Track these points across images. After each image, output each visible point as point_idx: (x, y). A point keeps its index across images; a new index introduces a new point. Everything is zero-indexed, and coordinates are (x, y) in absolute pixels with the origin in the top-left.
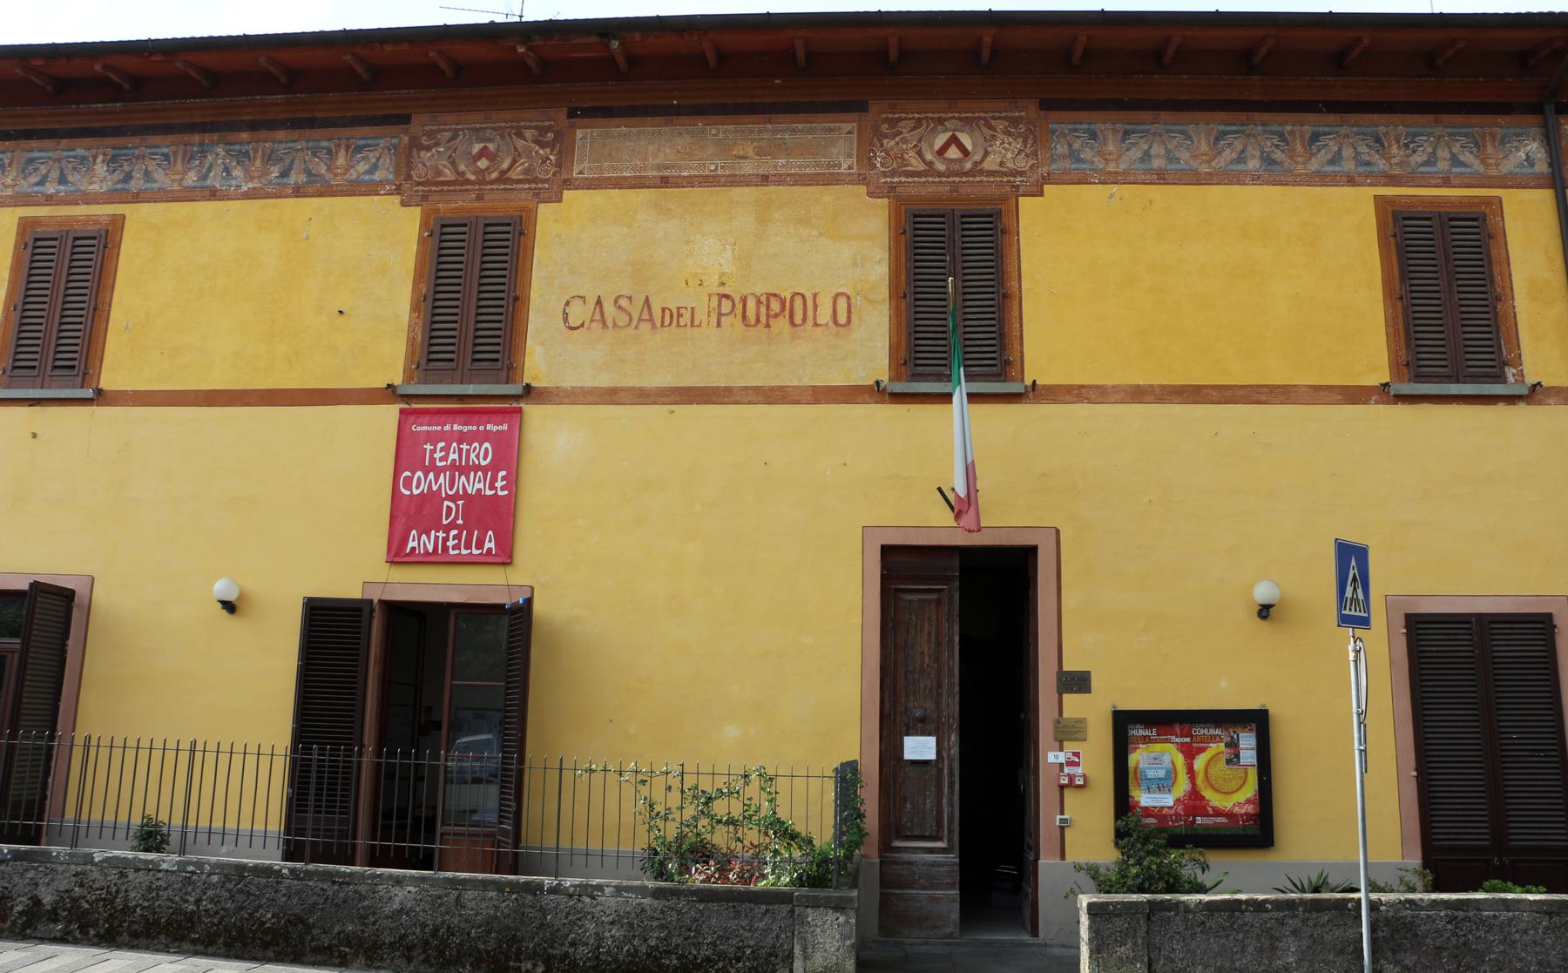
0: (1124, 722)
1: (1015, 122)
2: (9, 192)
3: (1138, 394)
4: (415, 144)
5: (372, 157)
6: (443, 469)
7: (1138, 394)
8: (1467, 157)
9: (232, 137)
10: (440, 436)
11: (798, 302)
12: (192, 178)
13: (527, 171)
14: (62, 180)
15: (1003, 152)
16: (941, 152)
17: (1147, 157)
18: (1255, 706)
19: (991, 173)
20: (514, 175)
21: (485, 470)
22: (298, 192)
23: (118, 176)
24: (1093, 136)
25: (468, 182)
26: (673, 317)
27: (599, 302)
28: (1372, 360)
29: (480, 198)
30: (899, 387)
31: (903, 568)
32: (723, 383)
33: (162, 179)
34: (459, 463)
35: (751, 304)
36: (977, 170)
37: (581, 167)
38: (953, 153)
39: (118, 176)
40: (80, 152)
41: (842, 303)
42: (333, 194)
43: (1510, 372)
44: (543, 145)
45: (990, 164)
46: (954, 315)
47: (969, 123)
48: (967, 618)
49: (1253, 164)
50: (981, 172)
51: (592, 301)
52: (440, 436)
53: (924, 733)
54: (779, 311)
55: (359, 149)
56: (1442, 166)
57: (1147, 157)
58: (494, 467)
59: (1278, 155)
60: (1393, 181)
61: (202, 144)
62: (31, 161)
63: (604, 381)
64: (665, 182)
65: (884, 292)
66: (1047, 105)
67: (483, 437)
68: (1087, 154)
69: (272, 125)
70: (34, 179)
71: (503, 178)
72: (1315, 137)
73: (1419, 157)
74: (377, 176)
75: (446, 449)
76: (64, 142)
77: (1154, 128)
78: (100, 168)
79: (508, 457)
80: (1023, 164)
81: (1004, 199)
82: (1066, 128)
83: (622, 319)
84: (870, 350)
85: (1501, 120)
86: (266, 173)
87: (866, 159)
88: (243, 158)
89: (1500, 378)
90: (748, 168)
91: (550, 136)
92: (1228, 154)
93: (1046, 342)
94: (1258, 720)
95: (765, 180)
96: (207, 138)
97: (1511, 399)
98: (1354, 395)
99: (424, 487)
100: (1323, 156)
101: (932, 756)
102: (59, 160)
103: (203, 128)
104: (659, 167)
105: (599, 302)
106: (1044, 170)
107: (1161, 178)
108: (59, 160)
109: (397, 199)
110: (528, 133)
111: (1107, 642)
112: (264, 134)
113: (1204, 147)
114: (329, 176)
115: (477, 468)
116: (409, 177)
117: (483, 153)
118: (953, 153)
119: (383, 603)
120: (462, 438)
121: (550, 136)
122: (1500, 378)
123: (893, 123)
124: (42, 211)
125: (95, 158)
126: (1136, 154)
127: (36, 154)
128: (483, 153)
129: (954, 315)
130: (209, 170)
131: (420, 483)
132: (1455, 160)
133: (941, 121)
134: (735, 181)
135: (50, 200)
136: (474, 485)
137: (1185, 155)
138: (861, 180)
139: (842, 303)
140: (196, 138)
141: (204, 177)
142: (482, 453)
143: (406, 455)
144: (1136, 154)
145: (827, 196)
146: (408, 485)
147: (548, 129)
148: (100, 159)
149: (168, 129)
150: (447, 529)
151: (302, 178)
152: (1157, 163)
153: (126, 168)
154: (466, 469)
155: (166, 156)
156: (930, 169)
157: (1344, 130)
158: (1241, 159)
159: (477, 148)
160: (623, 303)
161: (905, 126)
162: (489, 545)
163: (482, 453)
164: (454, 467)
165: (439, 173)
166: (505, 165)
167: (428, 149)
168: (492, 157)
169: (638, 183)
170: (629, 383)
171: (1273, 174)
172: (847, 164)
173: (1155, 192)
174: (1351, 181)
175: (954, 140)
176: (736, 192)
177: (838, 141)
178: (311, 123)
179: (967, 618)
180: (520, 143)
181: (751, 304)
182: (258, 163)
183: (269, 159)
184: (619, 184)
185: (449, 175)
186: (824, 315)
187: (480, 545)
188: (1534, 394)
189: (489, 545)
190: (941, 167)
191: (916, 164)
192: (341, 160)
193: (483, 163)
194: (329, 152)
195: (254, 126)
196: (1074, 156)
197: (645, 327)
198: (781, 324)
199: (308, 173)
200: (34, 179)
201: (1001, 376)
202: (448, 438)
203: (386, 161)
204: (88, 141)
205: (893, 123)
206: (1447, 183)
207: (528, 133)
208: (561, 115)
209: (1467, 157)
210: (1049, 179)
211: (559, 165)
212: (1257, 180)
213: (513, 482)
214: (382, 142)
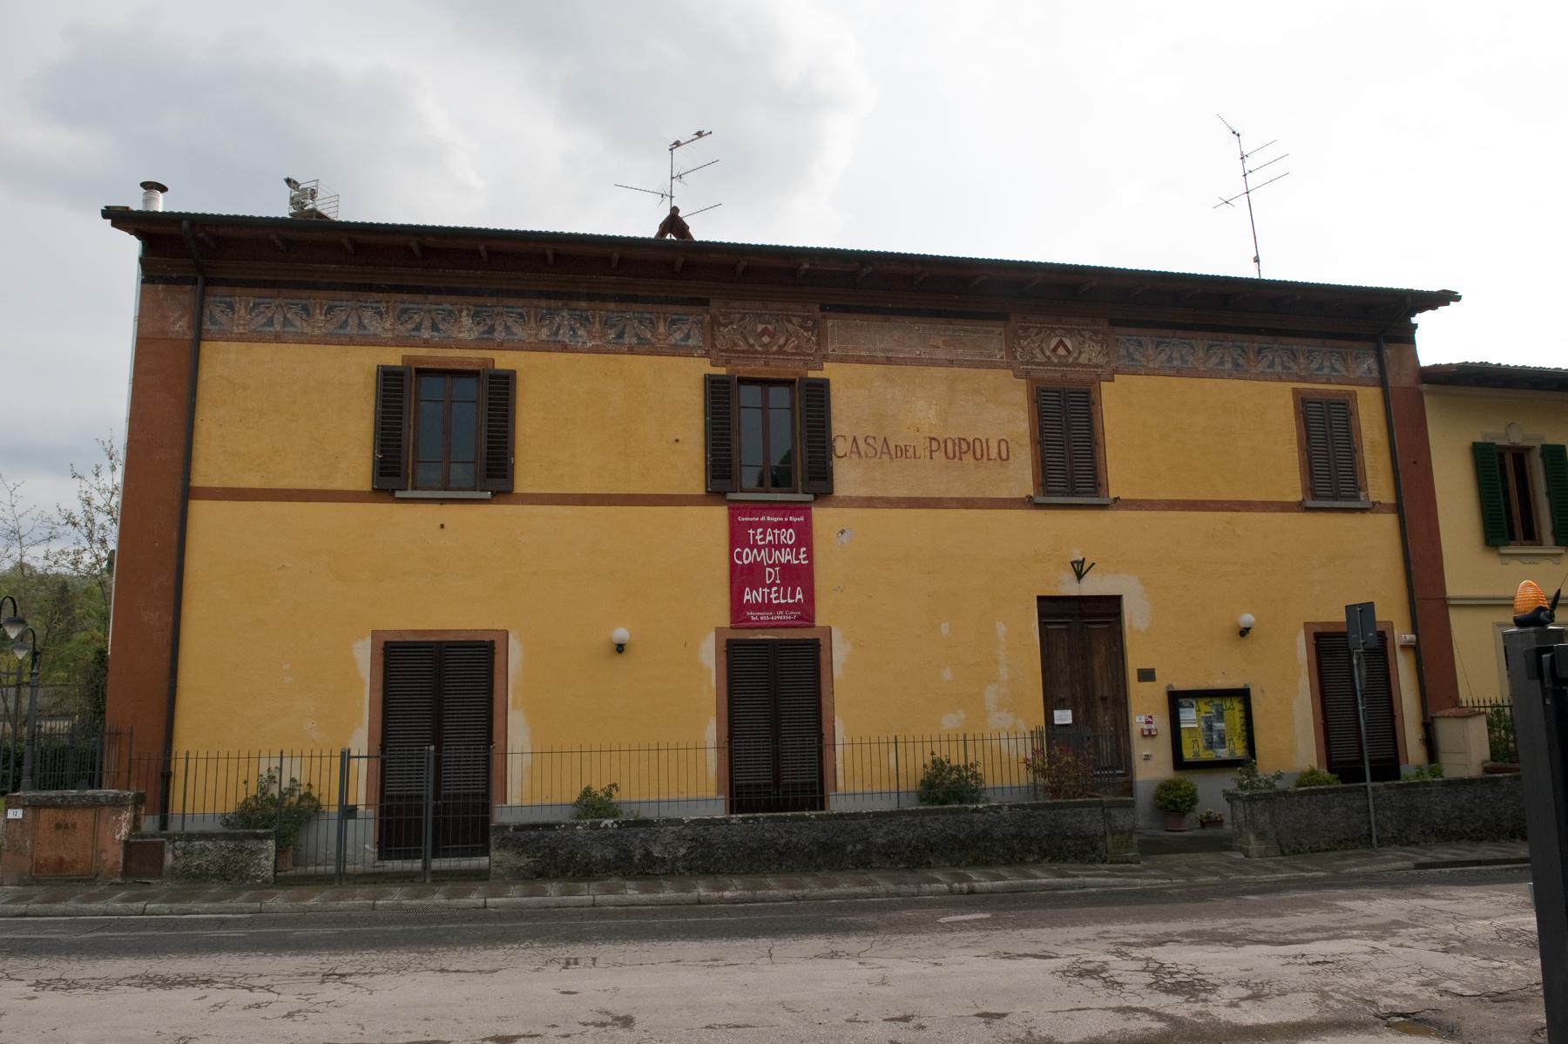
0: (1176, 699)
1: (1096, 332)
2: (390, 335)
3: (1172, 505)
4: (715, 322)
5: (685, 328)
6: (764, 546)
7: (1172, 505)
8: (1338, 366)
9: (574, 304)
10: (759, 524)
11: (978, 444)
12: (544, 334)
13: (797, 347)
14: (435, 328)
15: (1090, 353)
16: (1055, 350)
17: (1170, 359)
18: (1240, 685)
19: (1084, 366)
20: (788, 349)
21: (791, 547)
22: (632, 351)
23: (481, 328)
24: (1140, 344)
25: (756, 352)
26: (903, 452)
27: (854, 440)
28: (1293, 490)
29: (767, 364)
30: (1041, 500)
31: (1053, 610)
32: (937, 495)
33: (520, 332)
34: (773, 547)
35: (950, 444)
36: (1076, 364)
37: (833, 347)
38: (1061, 351)
39: (481, 328)
40: (446, 306)
41: (1003, 445)
42: (659, 354)
43: (1362, 494)
44: (806, 330)
45: (1083, 359)
46: (1069, 463)
47: (1069, 332)
48: (1080, 633)
49: (1228, 366)
50: (1079, 365)
51: (850, 440)
52: (759, 524)
53: (1065, 708)
54: (964, 450)
55: (673, 322)
56: (1326, 371)
57: (1170, 359)
58: (798, 545)
59: (1241, 361)
60: (1302, 379)
61: (549, 308)
62: (405, 311)
63: (863, 492)
64: (889, 361)
65: (1027, 440)
66: (1114, 323)
67: (788, 525)
68: (1137, 356)
69: (604, 298)
70: (410, 326)
71: (781, 350)
72: (1260, 351)
73: (1314, 366)
74: (691, 342)
75: (764, 533)
76: (432, 297)
77: (1175, 341)
78: (466, 321)
79: (805, 537)
80: (1101, 360)
81: (1093, 383)
82: (1124, 338)
83: (871, 452)
84: (1020, 477)
85: (1356, 344)
86: (605, 335)
87: (1011, 353)
88: (585, 321)
89: (1356, 498)
90: (940, 354)
91: (810, 323)
92: (1214, 360)
93: (1122, 472)
94: (1243, 695)
95: (951, 363)
96: (553, 303)
97: (1363, 510)
98: (1284, 507)
99: (751, 559)
100: (1265, 362)
101: (1070, 721)
102: (430, 312)
103: (549, 296)
104: (884, 350)
105: (854, 440)
106: (1113, 365)
107: (1179, 373)
108: (430, 312)
109: (708, 360)
110: (795, 320)
111: (1161, 645)
112: (598, 304)
113: (1201, 354)
114: (654, 340)
115: (786, 546)
116: (714, 346)
117: (765, 332)
118: (1061, 351)
119: (1544, 447)
120: (779, 526)
121: (810, 323)
122: (1356, 498)
123: (1026, 329)
124: (422, 352)
125: (460, 311)
126: (1163, 357)
127: (408, 306)
128: (765, 332)
129: (1069, 463)
130: (559, 328)
131: (748, 557)
132: (1333, 369)
133: (1053, 330)
134: (933, 363)
135: (426, 343)
136: (785, 557)
137: (1191, 359)
138: (1009, 366)
139: (1003, 445)
140: (544, 303)
141: (556, 333)
142: (789, 536)
143: (737, 537)
144: (1163, 357)
145: (988, 376)
146: (740, 556)
147: (808, 318)
148: (464, 313)
149: (518, 294)
150: (770, 587)
151: (634, 340)
152: (1176, 363)
153: (489, 322)
154: (779, 547)
155: (521, 316)
156: (1049, 362)
157: (1275, 347)
158: (1222, 363)
159: (760, 328)
160: (870, 441)
161: (1032, 332)
162: (799, 596)
163: (789, 536)
164: (770, 545)
165: (735, 344)
166: (782, 341)
167: (725, 326)
168: (772, 335)
169: (872, 361)
170: (880, 494)
171: (1239, 372)
172: (999, 355)
173: (1175, 381)
174: (1280, 379)
175: (1061, 343)
176: (934, 370)
177: (993, 340)
178: (634, 299)
179: (1080, 633)
180: (790, 327)
181: (950, 444)
182: (597, 326)
183: (606, 324)
184: (859, 360)
185: (742, 346)
186: (994, 453)
187: (793, 597)
188: (1118, 504)
189: (799, 596)
190: (1055, 360)
191: (1040, 358)
192: (662, 329)
193: (766, 339)
194: (652, 322)
195: (590, 297)
196: (1130, 357)
197: (886, 457)
198: (968, 458)
199: (637, 335)
200: (410, 326)
201: (1096, 493)
202: (766, 525)
203: (695, 332)
204: (453, 298)
205: (1026, 329)
206: (1329, 382)
207: (795, 320)
208: (816, 308)
209: (1338, 366)
210: (1116, 371)
211: (818, 344)
212: (1230, 376)
213: (810, 556)
214: (691, 318)
